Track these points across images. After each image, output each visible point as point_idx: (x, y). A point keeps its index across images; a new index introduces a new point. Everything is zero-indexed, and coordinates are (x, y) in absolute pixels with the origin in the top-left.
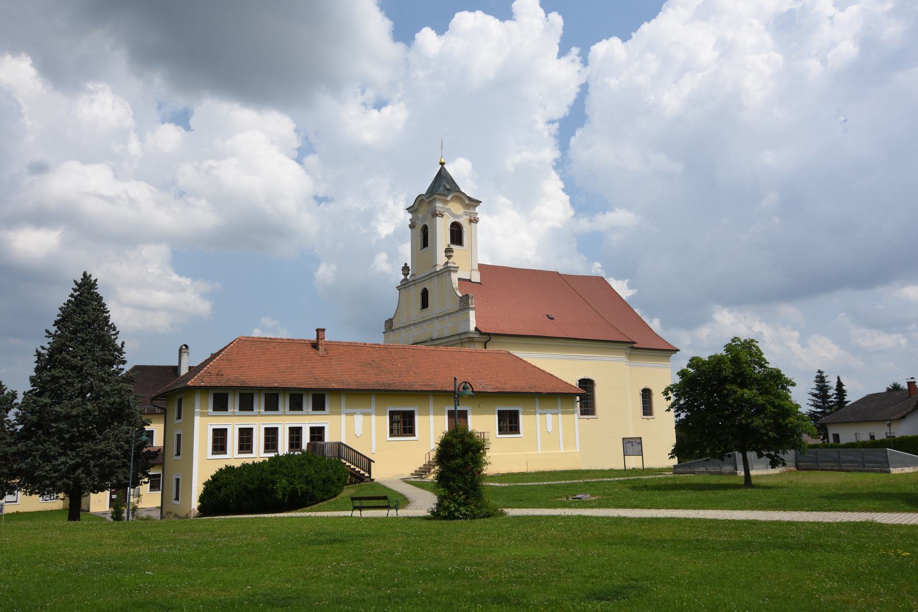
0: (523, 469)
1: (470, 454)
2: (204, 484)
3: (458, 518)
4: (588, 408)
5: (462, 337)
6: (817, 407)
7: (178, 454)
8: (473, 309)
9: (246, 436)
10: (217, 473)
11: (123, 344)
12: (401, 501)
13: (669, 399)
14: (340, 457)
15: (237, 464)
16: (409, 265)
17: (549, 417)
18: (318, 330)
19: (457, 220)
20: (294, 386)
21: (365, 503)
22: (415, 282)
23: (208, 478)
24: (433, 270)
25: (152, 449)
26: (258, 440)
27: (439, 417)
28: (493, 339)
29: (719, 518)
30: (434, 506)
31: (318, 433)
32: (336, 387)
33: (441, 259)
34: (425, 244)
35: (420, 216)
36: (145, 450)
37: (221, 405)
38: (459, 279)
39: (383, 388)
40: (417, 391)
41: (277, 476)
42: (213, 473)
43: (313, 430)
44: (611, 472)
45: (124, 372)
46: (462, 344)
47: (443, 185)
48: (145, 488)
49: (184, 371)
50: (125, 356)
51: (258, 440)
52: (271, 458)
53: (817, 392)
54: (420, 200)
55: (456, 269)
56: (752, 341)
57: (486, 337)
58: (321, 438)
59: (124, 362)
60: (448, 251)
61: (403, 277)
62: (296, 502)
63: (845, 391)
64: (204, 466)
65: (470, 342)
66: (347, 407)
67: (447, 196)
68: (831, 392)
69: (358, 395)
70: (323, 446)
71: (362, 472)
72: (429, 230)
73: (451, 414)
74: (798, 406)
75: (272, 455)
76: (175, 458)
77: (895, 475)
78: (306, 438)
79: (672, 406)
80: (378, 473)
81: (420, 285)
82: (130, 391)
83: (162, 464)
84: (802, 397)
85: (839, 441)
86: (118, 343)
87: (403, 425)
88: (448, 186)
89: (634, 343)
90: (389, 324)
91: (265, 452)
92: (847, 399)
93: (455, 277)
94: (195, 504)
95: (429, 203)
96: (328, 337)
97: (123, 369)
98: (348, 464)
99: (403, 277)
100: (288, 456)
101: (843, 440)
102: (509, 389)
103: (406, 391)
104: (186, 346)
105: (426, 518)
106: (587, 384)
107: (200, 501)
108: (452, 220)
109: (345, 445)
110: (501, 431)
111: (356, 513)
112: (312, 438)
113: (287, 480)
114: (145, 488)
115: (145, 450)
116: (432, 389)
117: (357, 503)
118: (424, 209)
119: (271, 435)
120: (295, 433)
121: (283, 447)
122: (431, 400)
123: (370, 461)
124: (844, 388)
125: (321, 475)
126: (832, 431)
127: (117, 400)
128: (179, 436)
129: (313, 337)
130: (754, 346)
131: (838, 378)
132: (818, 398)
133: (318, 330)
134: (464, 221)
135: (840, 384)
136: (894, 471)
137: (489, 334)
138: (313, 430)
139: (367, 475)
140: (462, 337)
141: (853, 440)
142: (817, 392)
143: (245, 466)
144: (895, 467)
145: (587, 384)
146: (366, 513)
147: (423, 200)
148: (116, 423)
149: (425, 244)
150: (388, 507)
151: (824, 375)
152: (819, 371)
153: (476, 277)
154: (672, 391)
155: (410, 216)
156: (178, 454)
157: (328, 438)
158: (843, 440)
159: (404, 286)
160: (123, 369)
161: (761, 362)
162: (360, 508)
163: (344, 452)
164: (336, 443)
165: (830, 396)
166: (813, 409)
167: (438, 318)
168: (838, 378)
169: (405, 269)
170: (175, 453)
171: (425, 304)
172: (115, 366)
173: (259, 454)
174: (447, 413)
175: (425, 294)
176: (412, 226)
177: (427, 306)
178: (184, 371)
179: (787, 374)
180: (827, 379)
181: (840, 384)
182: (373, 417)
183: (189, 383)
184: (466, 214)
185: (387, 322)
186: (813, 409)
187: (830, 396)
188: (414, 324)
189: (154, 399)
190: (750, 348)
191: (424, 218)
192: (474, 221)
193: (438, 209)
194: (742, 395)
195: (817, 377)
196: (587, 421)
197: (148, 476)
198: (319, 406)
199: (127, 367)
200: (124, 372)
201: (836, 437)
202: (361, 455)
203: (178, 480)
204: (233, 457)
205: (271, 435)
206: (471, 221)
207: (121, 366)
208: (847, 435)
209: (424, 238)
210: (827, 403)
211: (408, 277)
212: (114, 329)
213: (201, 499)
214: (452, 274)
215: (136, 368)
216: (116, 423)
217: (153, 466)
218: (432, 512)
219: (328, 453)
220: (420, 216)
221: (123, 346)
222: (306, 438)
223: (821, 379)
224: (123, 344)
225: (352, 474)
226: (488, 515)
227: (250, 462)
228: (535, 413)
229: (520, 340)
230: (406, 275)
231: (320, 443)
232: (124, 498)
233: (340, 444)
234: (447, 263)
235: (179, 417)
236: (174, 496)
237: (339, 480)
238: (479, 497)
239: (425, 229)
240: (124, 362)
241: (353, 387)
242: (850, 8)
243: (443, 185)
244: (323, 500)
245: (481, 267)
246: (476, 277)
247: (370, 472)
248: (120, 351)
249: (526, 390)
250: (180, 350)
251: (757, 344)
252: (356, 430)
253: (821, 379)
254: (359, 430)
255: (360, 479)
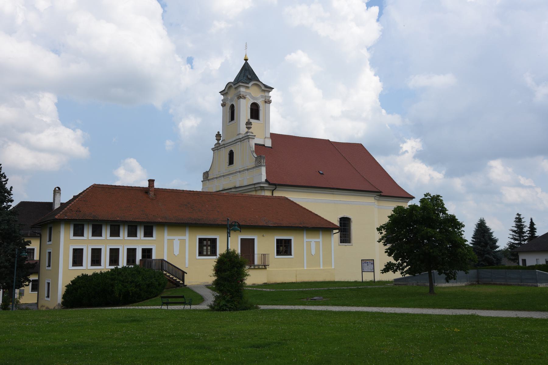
0: (293, 280)
1: (236, 269)
2: (66, 286)
3: (225, 310)
4: (345, 238)
5: (256, 186)
6: (515, 239)
7: (49, 266)
9: (96, 256)
10: (76, 279)
11: (11, 188)
12: (201, 299)
13: (381, 233)
14: (162, 269)
15: (90, 273)
16: (221, 133)
18: (149, 181)
19: (255, 101)
20: (131, 220)
21: (170, 300)
22: (224, 146)
23: (69, 282)
24: (237, 137)
25: (31, 262)
26: (105, 257)
29: (384, 312)
30: (212, 303)
31: (147, 253)
32: (161, 221)
34: (232, 118)
35: (229, 98)
36: (26, 262)
38: (256, 144)
41: (116, 282)
42: (73, 279)
43: (144, 250)
44: (356, 282)
45: (11, 208)
46: (256, 191)
47: (247, 75)
48: (27, 289)
49: (57, 206)
50: (13, 197)
51: (105, 257)
52: (112, 270)
53: (516, 229)
54: (229, 86)
56: (438, 196)
58: (150, 256)
59: (12, 201)
60: (248, 124)
61: (216, 142)
62: (127, 299)
63: (535, 229)
64: (65, 273)
65: (261, 190)
67: (248, 83)
68: (525, 229)
70: (151, 262)
71: (178, 280)
72: (235, 108)
74: (466, 241)
75: (113, 267)
76: (47, 268)
77: (541, 288)
78: (139, 256)
79: (383, 238)
80: (189, 281)
81: (226, 148)
82: (16, 221)
83: (37, 272)
84: (468, 234)
85: (525, 265)
86: (8, 186)
88: (249, 76)
89: (381, 192)
90: (206, 176)
91: (110, 265)
92: (537, 234)
93: (253, 143)
94: (60, 300)
95: (236, 88)
96: (157, 185)
97: (11, 206)
98: (168, 274)
99: (216, 142)
100: (124, 268)
101: (528, 264)
102: (285, 224)
104: (58, 188)
105: (207, 310)
106: (345, 222)
107: (63, 298)
108: (252, 101)
109: (166, 261)
110: (279, 253)
111: (164, 307)
112: (143, 256)
113: (122, 285)
114: (27, 289)
115: (26, 262)
117: (165, 300)
118: (232, 92)
119: (114, 254)
120: (131, 252)
121: (123, 262)
123: (184, 273)
124: (535, 226)
125: (150, 281)
126: (521, 257)
127: (6, 227)
128: (50, 253)
129: (146, 184)
130: (439, 199)
131: (531, 219)
132: (516, 233)
133: (149, 181)
134: (260, 102)
135: (532, 224)
136: (541, 285)
138: (144, 250)
139: (181, 282)
140: (256, 186)
141: (534, 263)
142: (516, 229)
143: (95, 275)
144: (541, 283)
145: (345, 222)
146: (171, 307)
147: (231, 86)
148: (5, 244)
149: (232, 118)
150: (184, 303)
151: (521, 217)
152: (518, 214)
153: (268, 143)
154: (384, 229)
156: (49, 266)
157: (155, 256)
158: (528, 264)
159: (217, 148)
160: (11, 206)
161: (444, 210)
162: (167, 304)
163: (165, 265)
164: (160, 260)
165: (525, 232)
166: (513, 241)
167: (240, 172)
168: (531, 219)
169: (218, 136)
170: (47, 265)
171: (231, 162)
172: (5, 204)
173: (105, 266)
175: (231, 154)
176: (223, 105)
177: (233, 163)
178: (57, 206)
179: (460, 219)
180: (523, 220)
181: (532, 224)
183: (56, 217)
184: (262, 97)
185: (204, 173)
186: (513, 241)
187: (525, 232)
188: (223, 176)
189: (33, 227)
190: (437, 199)
191: (232, 100)
192: (268, 102)
193: (242, 93)
194: (427, 233)
195: (516, 218)
196: (345, 247)
197: (29, 281)
199: (14, 205)
200: (11, 208)
201: (524, 261)
202: (177, 268)
203: (49, 284)
204: (87, 268)
205: (114, 254)
206: (266, 102)
207: (9, 204)
208: (531, 260)
209: (232, 113)
210: (523, 237)
211: (220, 142)
212: (5, 177)
213: (64, 297)
215: (23, 204)
216: (5, 244)
217: (32, 274)
218: (211, 306)
219: (154, 267)
220: (229, 98)
221: (11, 190)
222: (139, 256)
223: (519, 220)
224: (11, 188)
225: (169, 280)
226: (245, 309)
227: (99, 272)
230: (218, 140)
231: (148, 259)
232: (12, 295)
233: (162, 261)
234: (247, 132)
235: (50, 240)
236: (46, 295)
237: (159, 285)
238: (241, 297)
239: (232, 107)
240: (12, 201)
241: (173, 221)
242: (135, 161)
243: (247, 75)
244: (148, 298)
245: (273, 136)
246: (268, 143)
248: (9, 193)
249: (297, 225)
250: (55, 191)
251: (441, 198)
252: (176, 249)
253: (519, 220)
255: (177, 285)
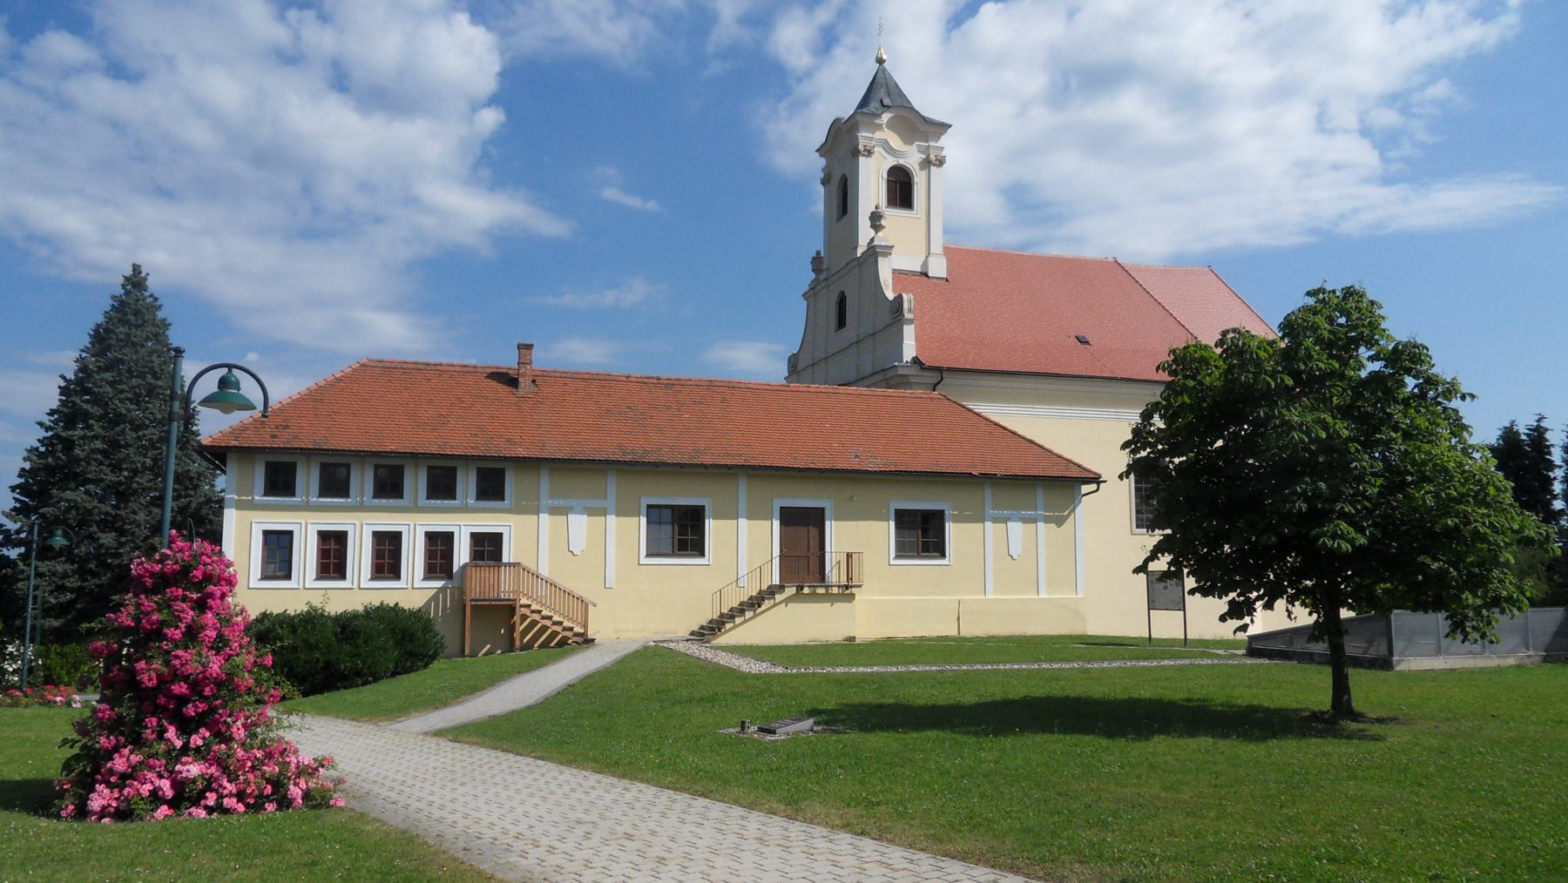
8: (910, 322)
17: (1015, 527)
19: (902, 162)
27: (630, 521)
28: (948, 379)
31: (488, 547)
33: (865, 233)
37: (280, 482)
39: (629, 458)
40: (705, 466)
43: (477, 539)
55: (887, 251)
57: (934, 374)
66: (552, 497)
69: (580, 473)
73: (789, 517)
78: (462, 554)
87: (683, 532)
96: (542, 359)
103: (681, 466)
108: (892, 161)
116: (742, 462)
122: (988, 492)
137: (940, 370)
138: (477, 539)
155: (822, 162)
174: (777, 513)
180: (1548, 435)
181: (1309, 294)
182: (612, 520)
198: (491, 488)
214: (880, 259)
222: (462, 554)
228: (981, 519)
229: (1030, 384)
247: (585, 626)
254: (579, 544)
